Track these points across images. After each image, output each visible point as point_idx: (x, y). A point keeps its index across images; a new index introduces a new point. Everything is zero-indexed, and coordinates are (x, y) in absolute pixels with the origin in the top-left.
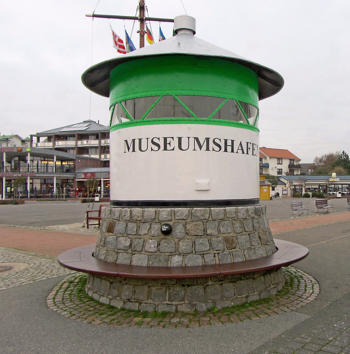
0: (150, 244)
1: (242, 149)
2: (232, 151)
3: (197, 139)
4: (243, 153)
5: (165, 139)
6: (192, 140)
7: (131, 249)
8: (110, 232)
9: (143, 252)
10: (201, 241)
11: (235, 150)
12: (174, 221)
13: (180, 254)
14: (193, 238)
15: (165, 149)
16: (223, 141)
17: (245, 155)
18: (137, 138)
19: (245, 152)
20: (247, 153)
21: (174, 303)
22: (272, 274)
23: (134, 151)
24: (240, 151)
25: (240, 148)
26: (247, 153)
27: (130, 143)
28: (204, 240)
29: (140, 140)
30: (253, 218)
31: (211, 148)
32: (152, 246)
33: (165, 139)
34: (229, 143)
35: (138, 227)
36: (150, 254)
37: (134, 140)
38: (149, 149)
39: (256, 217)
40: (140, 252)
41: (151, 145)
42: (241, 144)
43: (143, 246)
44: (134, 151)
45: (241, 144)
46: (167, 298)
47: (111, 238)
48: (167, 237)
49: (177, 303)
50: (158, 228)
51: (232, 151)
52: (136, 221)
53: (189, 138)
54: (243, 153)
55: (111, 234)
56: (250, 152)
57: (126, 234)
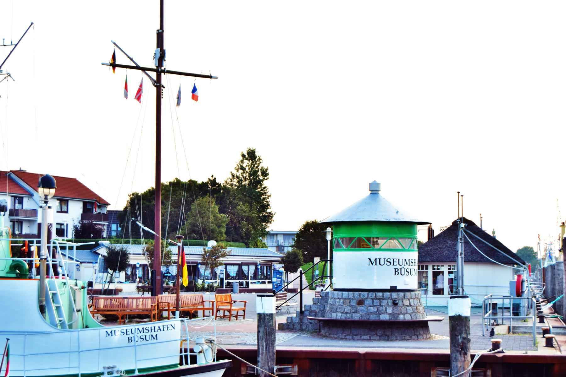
11: (156, 330)
18: (378, 258)
19: (162, 329)
29: (380, 259)
36: (390, 314)
37: (376, 259)
43: (386, 311)
47: (361, 307)
57: (374, 306)
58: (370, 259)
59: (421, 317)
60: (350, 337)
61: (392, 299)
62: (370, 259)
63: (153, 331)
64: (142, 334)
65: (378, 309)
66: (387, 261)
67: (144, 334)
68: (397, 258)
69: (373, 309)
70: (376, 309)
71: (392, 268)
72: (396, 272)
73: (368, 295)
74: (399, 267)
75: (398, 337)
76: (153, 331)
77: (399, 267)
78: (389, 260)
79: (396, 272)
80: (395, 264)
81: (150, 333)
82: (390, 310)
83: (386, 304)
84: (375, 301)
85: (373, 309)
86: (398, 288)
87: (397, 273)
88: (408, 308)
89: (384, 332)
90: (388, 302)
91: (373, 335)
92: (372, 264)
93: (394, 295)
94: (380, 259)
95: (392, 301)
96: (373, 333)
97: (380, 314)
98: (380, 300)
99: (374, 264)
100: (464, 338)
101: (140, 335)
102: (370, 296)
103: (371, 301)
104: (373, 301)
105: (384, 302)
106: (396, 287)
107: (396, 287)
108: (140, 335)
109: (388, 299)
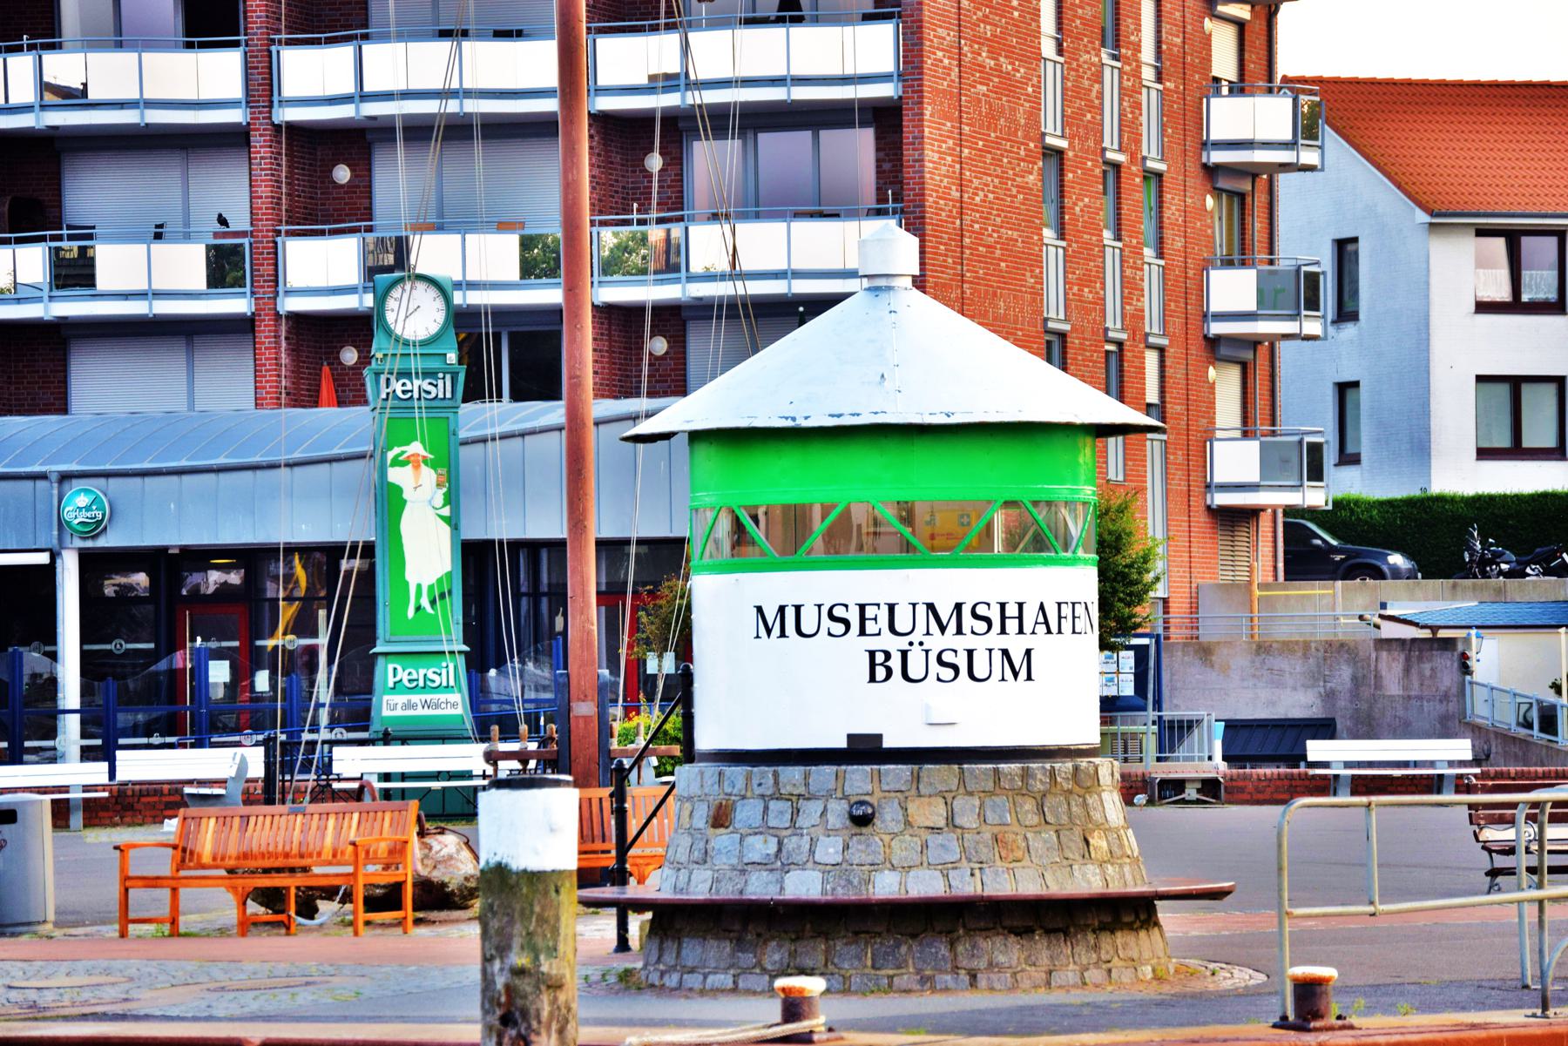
0: (827, 848)
1: (1046, 622)
2: (1021, 631)
3: (931, 607)
4: (1049, 632)
5: (862, 607)
6: (922, 610)
7: (780, 863)
8: (722, 826)
9: (810, 865)
10: (940, 839)
11: (1028, 627)
12: (878, 794)
13: (893, 868)
14: (926, 835)
15: (862, 632)
16: (996, 610)
17: (1054, 637)
18: (790, 601)
19: (1054, 628)
20: (1060, 632)
21: (883, 972)
22: (1119, 934)
23: (783, 634)
24: (1042, 629)
25: (1041, 619)
26: (1060, 632)
27: (771, 614)
28: (950, 839)
29: (798, 608)
30: (1070, 792)
31: (966, 629)
32: (831, 850)
33: (862, 607)
34: (1012, 610)
35: (796, 812)
36: (827, 869)
37: (782, 609)
38: (823, 631)
39: (1077, 789)
40: (802, 866)
41: (934, 667)
42: (1042, 607)
43: (812, 852)
44: (783, 634)
45: (1042, 607)
46: (869, 963)
47: (722, 840)
48: (864, 830)
49: (891, 972)
50: (1150, 544)
51: (1021, 631)
52: (788, 798)
53: (914, 605)
54: (1049, 632)
55: (722, 830)
56: (1067, 625)
57: (764, 829)
58: (760, 609)
59: (1084, 884)
60: (725, 980)
61: (845, 797)
62: (760, 609)
63: (1012, 625)
64: (949, 639)
65: (780, 843)
66: (832, 617)
67: (962, 643)
68: (884, 600)
69: (760, 847)
70: (772, 848)
71: (855, 648)
72: (878, 668)
73: (749, 778)
74: (894, 644)
75: (856, 980)
76: (1012, 625)
77: (894, 644)
78: (838, 612)
79: (878, 668)
80: (870, 627)
81: (995, 640)
82: (829, 850)
83: (815, 819)
84: (773, 805)
85: (760, 847)
86: (887, 744)
87: (881, 673)
88: (934, 840)
89: (793, 954)
90: (824, 813)
91: (747, 970)
92: (769, 631)
93: (859, 778)
94: (798, 608)
95: (844, 805)
96: (747, 959)
97: (786, 868)
98: (796, 801)
99: (776, 631)
100: (519, 972)
101: (937, 642)
102: (755, 782)
103: (760, 805)
104: (766, 809)
105: (812, 810)
106: (879, 737)
107: (879, 737)
108: (937, 642)
109: (829, 795)
